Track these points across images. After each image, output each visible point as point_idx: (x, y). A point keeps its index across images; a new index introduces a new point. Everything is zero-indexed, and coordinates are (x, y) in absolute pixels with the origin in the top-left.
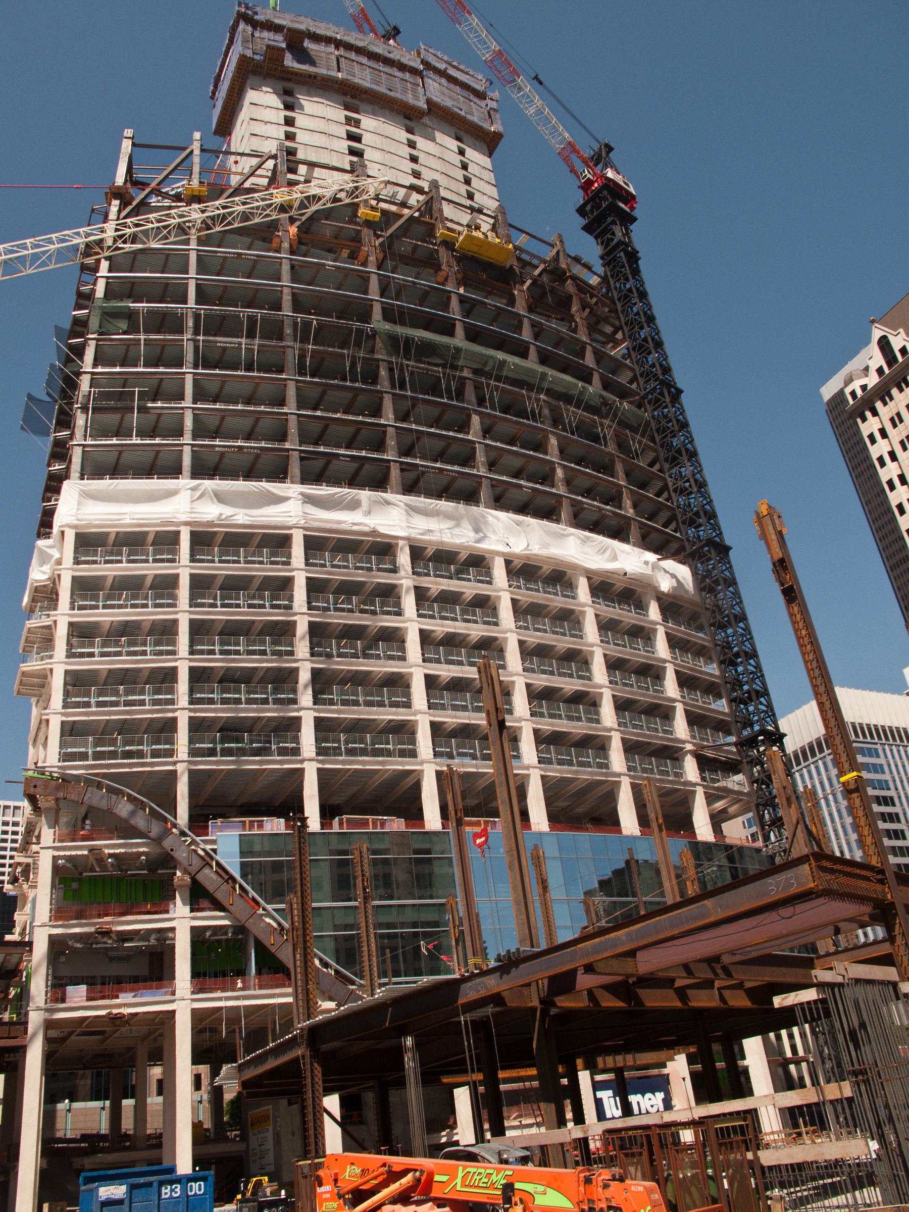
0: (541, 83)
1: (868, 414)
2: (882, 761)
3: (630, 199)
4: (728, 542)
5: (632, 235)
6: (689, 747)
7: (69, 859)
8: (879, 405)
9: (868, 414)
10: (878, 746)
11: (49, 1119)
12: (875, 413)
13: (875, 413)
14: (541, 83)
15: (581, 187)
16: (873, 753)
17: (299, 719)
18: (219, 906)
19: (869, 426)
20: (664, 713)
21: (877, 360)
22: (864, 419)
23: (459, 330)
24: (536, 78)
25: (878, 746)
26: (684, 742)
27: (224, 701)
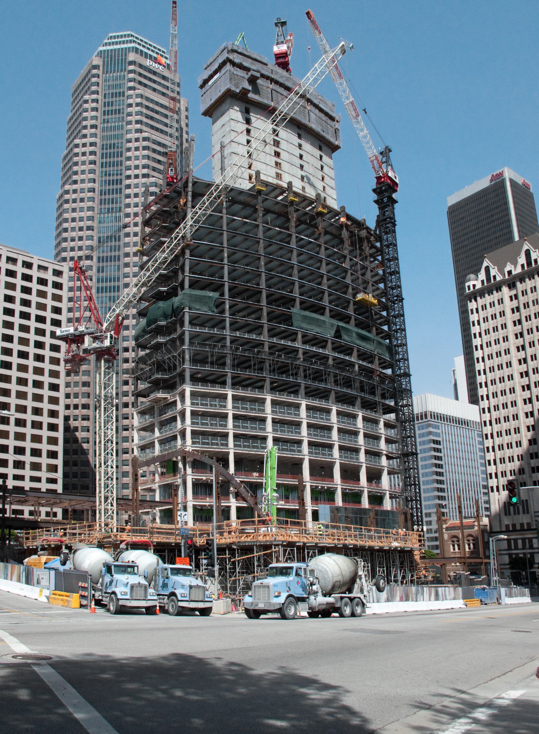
0: (366, 113)
1: (473, 300)
2: (440, 431)
3: (396, 184)
4: (411, 373)
5: (396, 211)
6: (384, 452)
7: (195, 479)
8: (478, 298)
9: (473, 300)
10: (440, 424)
11: (520, 549)
12: (476, 300)
13: (476, 300)
14: (366, 113)
15: (376, 178)
16: (437, 427)
17: (267, 436)
18: (244, 500)
19: (472, 305)
20: (377, 438)
21: (482, 275)
22: (471, 301)
23: (353, 321)
24: (364, 110)
25: (440, 424)
26: (383, 450)
27: (202, 404)
